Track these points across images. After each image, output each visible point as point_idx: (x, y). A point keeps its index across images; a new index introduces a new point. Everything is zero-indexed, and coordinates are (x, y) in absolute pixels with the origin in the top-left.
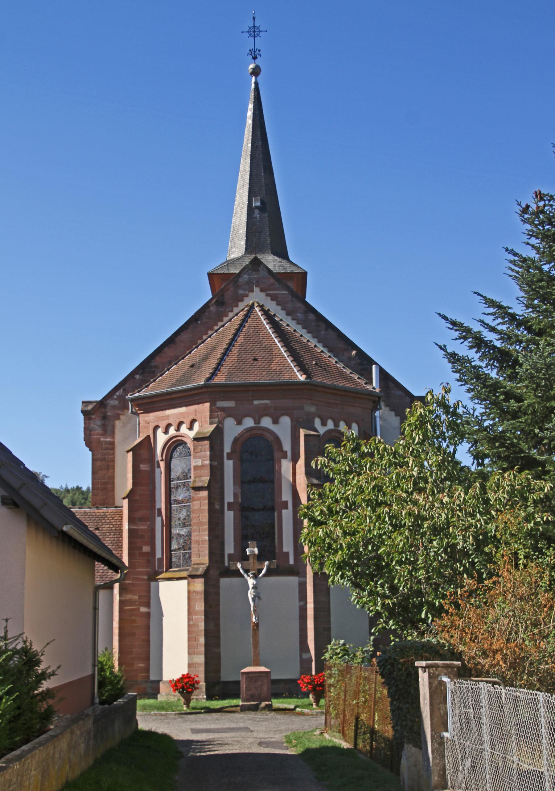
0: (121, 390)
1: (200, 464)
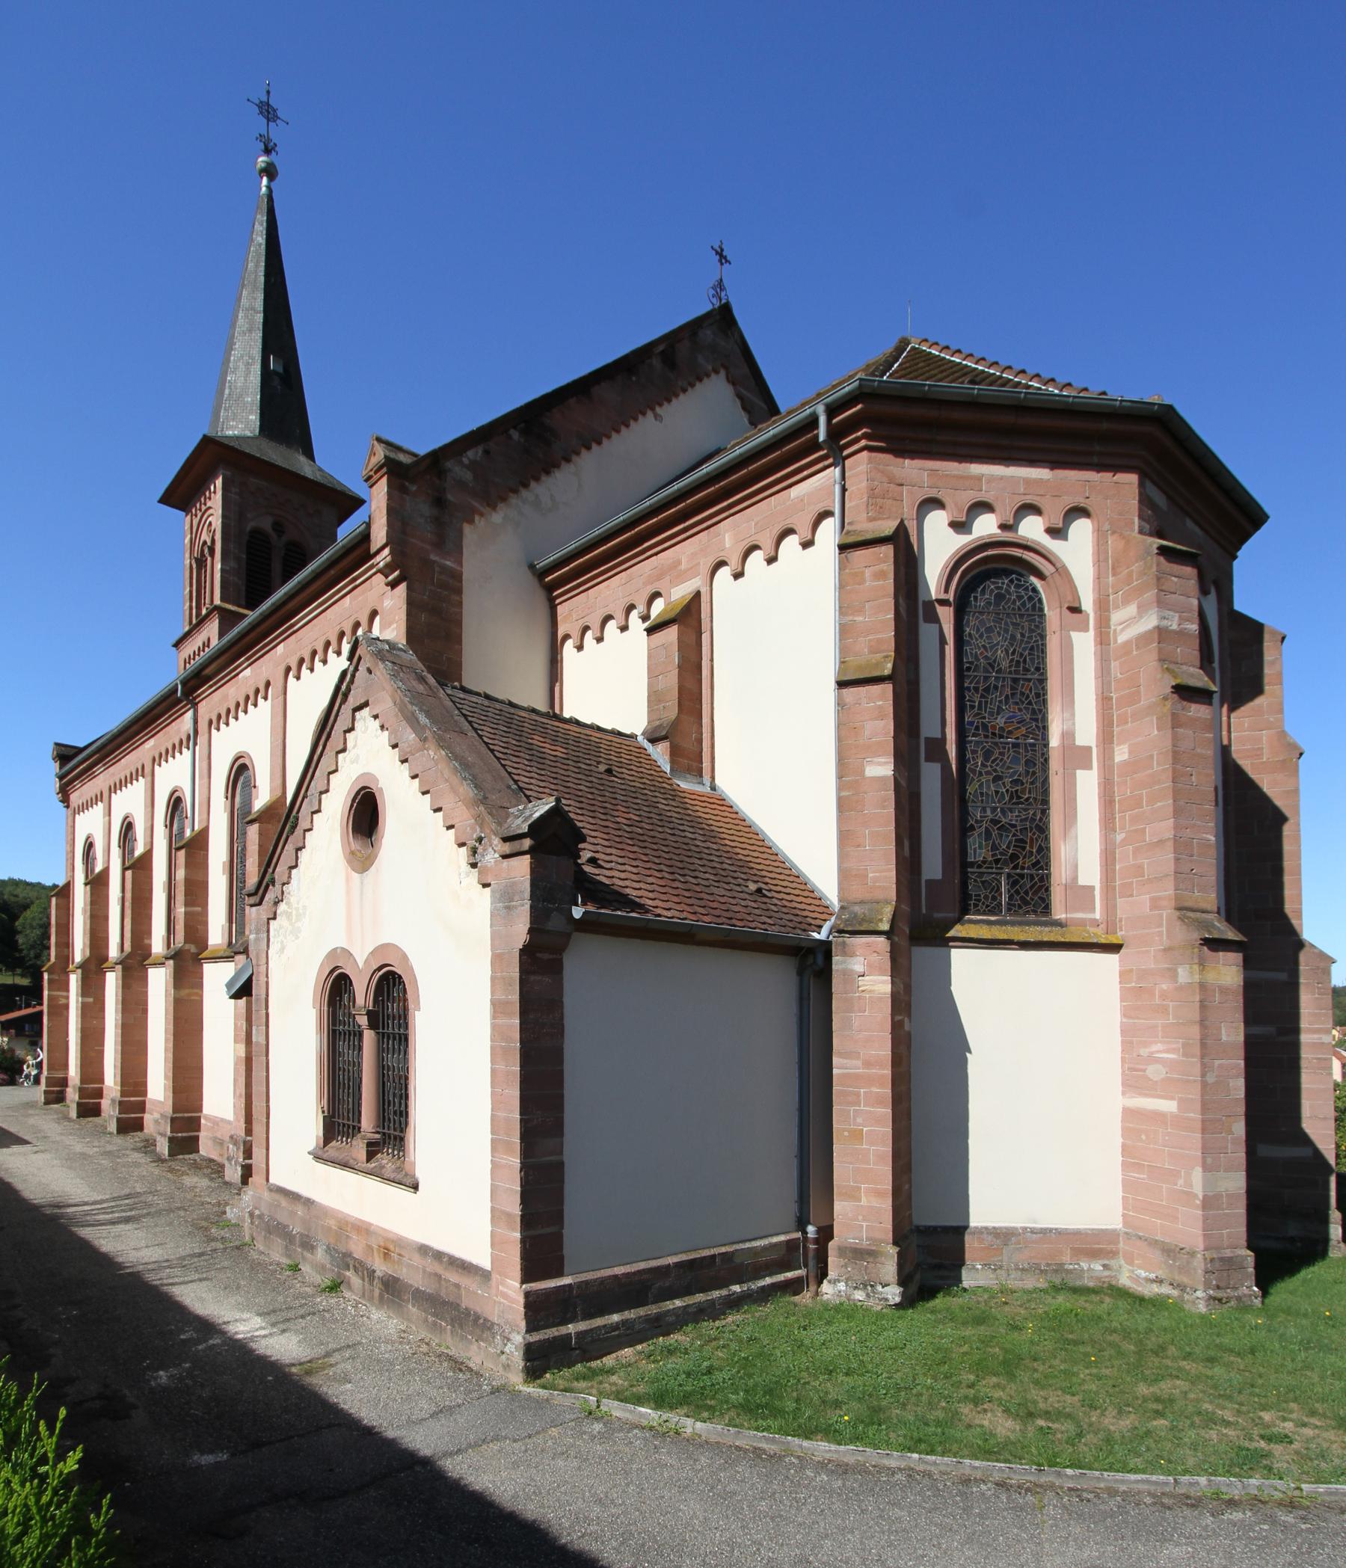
0: (480, 450)
1: (1175, 627)
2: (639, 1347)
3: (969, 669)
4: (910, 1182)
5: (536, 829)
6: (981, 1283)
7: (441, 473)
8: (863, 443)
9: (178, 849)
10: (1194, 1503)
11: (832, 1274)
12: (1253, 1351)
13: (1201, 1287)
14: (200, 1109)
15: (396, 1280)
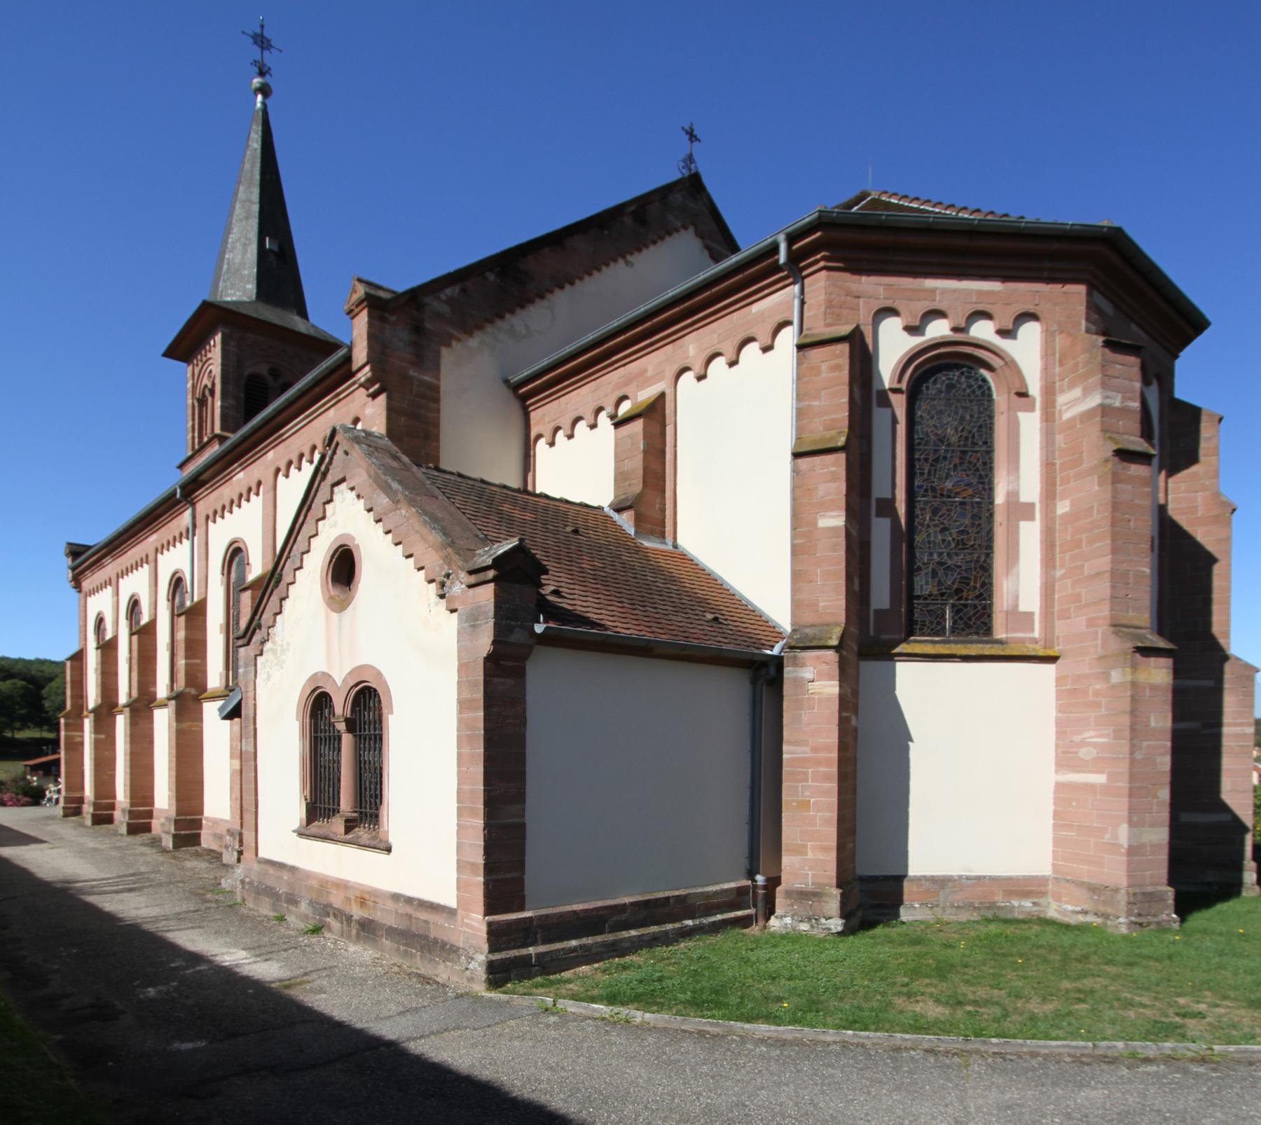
1: (1117, 404)
2: (596, 965)
3: (919, 444)
4: (854, 842)
5: (498, 562)
6: (919, 918)
7: (420, 307)
8: (822, 264)
9: (179, 615)
10: (1113, 1061)
11: (779, 911)
12: (1170, 957)
13: (1124, 914)
14: (201, 812)
15: (372, 921)
